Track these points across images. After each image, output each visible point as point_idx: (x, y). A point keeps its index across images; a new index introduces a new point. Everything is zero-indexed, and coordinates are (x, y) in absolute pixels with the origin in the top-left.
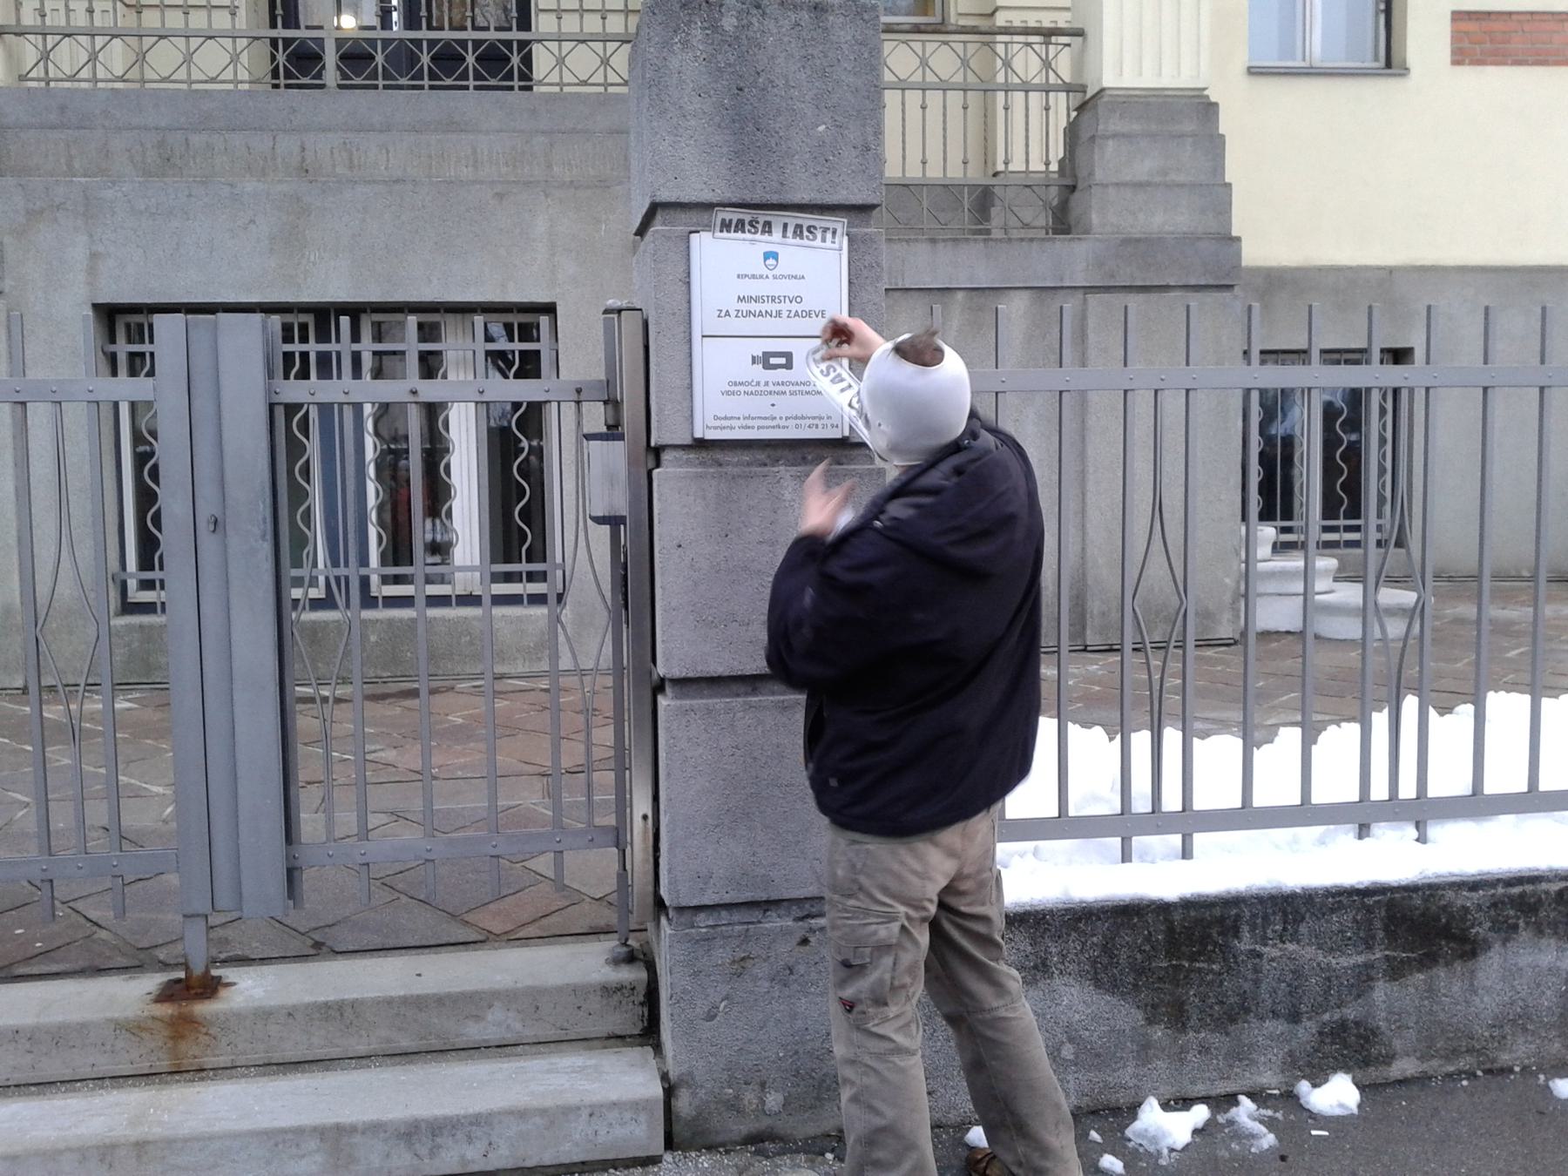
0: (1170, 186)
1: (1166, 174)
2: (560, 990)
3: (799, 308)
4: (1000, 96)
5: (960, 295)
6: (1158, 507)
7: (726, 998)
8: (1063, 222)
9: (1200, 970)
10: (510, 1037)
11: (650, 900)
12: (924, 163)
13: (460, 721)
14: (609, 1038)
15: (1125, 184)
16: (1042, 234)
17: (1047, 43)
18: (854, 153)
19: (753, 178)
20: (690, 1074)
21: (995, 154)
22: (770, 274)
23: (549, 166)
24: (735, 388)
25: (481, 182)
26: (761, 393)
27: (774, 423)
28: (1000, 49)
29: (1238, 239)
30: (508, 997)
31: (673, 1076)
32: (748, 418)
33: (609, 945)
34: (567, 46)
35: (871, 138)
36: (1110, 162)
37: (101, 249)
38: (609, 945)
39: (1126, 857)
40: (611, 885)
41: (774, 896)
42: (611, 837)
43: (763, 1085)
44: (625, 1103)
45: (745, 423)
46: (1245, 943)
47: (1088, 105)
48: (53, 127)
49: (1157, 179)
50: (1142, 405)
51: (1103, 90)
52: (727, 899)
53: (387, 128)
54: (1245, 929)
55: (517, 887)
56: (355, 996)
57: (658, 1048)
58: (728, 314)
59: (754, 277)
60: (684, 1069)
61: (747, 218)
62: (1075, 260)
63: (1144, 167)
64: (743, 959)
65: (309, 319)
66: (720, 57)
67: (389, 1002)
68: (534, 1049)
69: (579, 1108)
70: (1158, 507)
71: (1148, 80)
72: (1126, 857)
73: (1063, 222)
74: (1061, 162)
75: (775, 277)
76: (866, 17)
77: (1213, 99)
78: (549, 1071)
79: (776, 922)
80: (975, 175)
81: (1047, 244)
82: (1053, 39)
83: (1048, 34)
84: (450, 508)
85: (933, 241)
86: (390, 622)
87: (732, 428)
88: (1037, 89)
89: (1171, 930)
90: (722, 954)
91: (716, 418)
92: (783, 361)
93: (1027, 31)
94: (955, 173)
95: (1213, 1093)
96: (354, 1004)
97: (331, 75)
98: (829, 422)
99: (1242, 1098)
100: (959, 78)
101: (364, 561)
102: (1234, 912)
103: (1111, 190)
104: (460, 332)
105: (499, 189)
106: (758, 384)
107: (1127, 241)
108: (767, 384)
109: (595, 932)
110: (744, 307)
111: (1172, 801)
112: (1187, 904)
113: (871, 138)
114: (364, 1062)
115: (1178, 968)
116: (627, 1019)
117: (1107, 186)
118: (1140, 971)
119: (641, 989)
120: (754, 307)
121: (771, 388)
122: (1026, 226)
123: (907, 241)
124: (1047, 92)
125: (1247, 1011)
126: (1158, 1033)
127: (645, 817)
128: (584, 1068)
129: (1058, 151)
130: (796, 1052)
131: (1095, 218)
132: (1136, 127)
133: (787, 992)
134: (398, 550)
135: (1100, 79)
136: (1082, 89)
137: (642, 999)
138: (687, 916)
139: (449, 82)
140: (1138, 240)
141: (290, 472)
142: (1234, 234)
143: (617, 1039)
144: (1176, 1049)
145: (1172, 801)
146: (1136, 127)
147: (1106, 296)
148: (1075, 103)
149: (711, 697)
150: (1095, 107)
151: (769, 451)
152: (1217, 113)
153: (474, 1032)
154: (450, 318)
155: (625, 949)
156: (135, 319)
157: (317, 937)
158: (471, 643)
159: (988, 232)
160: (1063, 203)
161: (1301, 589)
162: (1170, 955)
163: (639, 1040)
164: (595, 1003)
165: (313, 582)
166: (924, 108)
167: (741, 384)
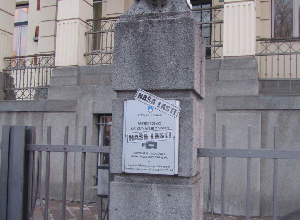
3: (160, 126)
18: (183, 71)
19: (146, 81)
24: (136, 155)
26: (145, 157)
27: (149, 168)
32: (140, 166)
35: (189, 66)
37: (95, 101)
45: (138, 167)
48: (90, 74)
58: (134, 128)
59: (144, 115)
61: (148, 96)
76: (189, 23)
87: (134, 169)
91: (129, 165)
92: (153, 145)
98: (169, 169)
106: (144, 153)
108: (147, 154)
110: (140, 126)
113: (189, 66)
120: (143, 126)
121: (148, 155)
123: (294, 96)
156: (103, 117)
167: (138, 153)
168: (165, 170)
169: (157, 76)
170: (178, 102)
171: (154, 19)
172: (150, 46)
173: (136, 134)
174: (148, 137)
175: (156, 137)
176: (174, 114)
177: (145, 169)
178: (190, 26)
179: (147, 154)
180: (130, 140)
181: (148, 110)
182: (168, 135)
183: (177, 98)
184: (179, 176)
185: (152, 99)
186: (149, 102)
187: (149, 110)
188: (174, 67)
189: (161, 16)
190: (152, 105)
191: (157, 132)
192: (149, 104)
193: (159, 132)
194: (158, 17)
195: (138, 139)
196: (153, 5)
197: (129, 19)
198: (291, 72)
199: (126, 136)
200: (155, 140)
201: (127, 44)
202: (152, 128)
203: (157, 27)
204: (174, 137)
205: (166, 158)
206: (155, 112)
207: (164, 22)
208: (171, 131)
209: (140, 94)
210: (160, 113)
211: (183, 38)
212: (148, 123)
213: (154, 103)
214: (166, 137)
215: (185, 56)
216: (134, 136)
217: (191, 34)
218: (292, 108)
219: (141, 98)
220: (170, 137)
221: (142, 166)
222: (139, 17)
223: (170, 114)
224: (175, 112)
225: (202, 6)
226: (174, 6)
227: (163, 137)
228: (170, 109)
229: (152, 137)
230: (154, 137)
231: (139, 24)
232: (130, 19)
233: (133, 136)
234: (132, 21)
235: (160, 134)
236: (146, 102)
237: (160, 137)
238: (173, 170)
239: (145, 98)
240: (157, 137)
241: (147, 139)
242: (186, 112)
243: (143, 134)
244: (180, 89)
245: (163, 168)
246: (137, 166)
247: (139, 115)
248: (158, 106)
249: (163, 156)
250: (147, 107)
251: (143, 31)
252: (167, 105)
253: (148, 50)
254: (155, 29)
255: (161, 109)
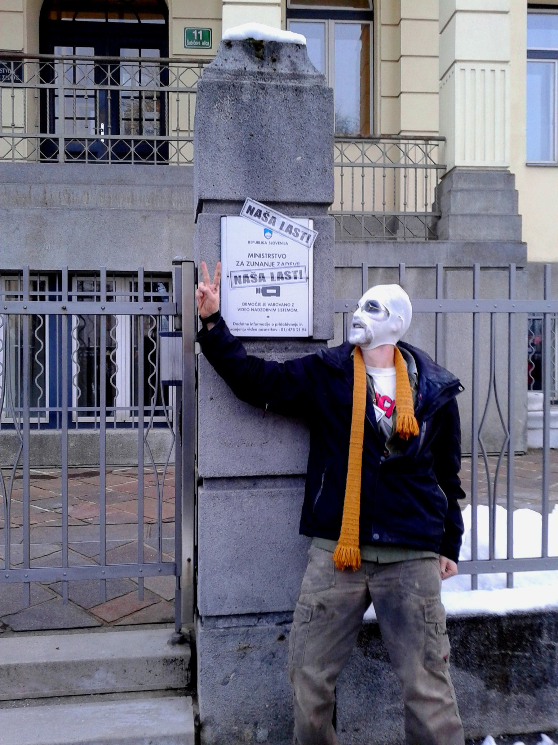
0: (489, 216)
1: (487, 210)
2: (139, 661)
3: (284, 261)
4: (402, 170)
5: (381, 270)
6: (493, 381)
7: (235, 671)
8: (434, 234)
9: (518, 657)
10: (108, 688)
11: (191, 609)
12: (363, 204)
13: (111, 490)
14: (167, 689)
15: (466, 215)
16: (423, 240)
17: (426, 144)
19: (258, 186)
20: (212, 717)
21: (399, 192)
22: (268, 241)
23: (171, 203)
24: (245, 307)
25: (135, 210)
26: (262, 310)
27: (269, 327)
28: (402, 147)
29: (525, 244)
30: (109, 664)
31: (202, 718)
33: (169, 632)
34: (181, 143)
36: (457, 204)
38: (169, 632)
39: (474, 586)
40: (172, 595)
41: (265, 610)
42: (172, 569)
43: (256, 724)
44: (171, 736)
45: (251, 327)
46: (545, 640)
47: (447, 175)
49: (483, 212)
50: (483, 322)
51: (455, 167)
52: (236, 612)
53: (88, 183)
54: (545, 632)
55: (125, 592)
56: (17, 662)
57: (195, 697)
59: (258, 242)
60: (208, 714)
62: (440, 253)
63: (477, 206)
64: (245, 648)
65: (46, 279)
66: (240, 117)
67: (37, 666)
68: (122, 696)
69: (143, 739)
70: (493, 381)
71: (478, 162)
72: (474, 586)
73: (434, 234)
74: (433, 205)
75: (270, 243)
76: (325, 96)
77: (512, 172)
78: (129, 712)
79: (265, 625)
80: (389, 210)
81: (427, 245)
82: (430, 142)
83: (427, 139)
84: (115, 376)
85: (367, 243)
86: (81, 436)
87: (243, 330)
88: (421, 167)
89: (500, 632)
90: (232, 645)
92: (274, 291)
93: (416, 138)
94: (379, 208)
95: (526, 731)
96: (16, 667)
97: (62, 157)
98: (301, 327)
99: (544, 737)
100: (381, 161)
101: (70, 404)
102: (539, 621)
103: (459, 218)
104: (123, 285)
105: (144, 214)
106: (260, 304)
107: (468, 244)
108: (265, 304)
109: (165, 622)
110: (252, 260)
111: (501, 553)
112: (512, 617)
114: (20, 703)
115: (505, 656)
116: (177, 679)
117: (457, 215)
118: (482, 657)
119: (187, 661)
120: (257, 260)
121: (267, 307)
122: (415, 236)
123: (353, 243)
124: (426, 169)
125: (546, 681)
126: (493, 694)
127: (189, 560)
128: (149, 711)
129: (432, 199)
130: (277, 705)
131: (451, 232)
132: (472, 186)
133: (271, 668)
134: (87, 399)
135: (454, 162)
136: (445, 168)
137: (187, 667)
138: (210, 623)
139: (121, 160)
140: (473, 244)
141: (32, 356)
142: (523, 241)
143: (172, 691)
144: (503, 705)
145: (501, 553)
146: (472, 186)
147: (456, 272)
148: (441, 175)
149: (227, 489)
150: (451, 176)
151: (267, 344)
152: (513, 179)
153: (87, 685)
154: (118, 280)
155: (179, 636)
157: (5, 621)
158: (123, 447)
159: (395, 239)
160: (434, 226)
161: (542, 426)
162: (500, 647)
163: (184, 692)
164: (159, 669)
165: (42, 414)
166: (363, 176)
168: (294, 330)
169: (275, 179)
170: (311, 222)
171: (265, 81)
172: (262, 127)
173: (245, 273)
174: (266, 279)
175: (278, 278)
176: (307, 242)
177: (262, 330)
178: (327, 100)
179: (265, 304)
180: (236, 283)
181: (264, 234)
182: (298, 275)
183: (311, 217)
184: (315, 338)
185: (271, 216)
186: (266, 221)
187: (266, 234)
188: (302, 165)
189: (278, 78)
190: (271, 226)
191: (280, 270)
192: (266, 224)
193: (283, 271)
194: (272, 79)
195: (249, 282)
196: (258, 57)
197: (221, 76)
198: (344, 200)
199: (228, 277)
200: (277, 282)
201: (222, 120)
202: (272, 264)
203: (273, 96)
204: (308, 278)
205: (296, 310)
206: (276, 237)
207: (285, 89)
208: (303, 269)
209: (250, 207)
210: (284, 240)
211: (317, 119)
212: (265, 255)
213: (274, 222)
214: (295, 278)
215: (321, 149)
216: (242, 276)
217: (330, 114)
218: (350, 266)
219: (251, 214)
220: (301, 278)
221: (256, 325)
222: (239, 75)
223: (300, 241)
224: (308, 239)
225: (77, 48)
226: (293, 63)
227: (290, 278)
228: (301, 234)
229: (272, 277)
230: (276, 278)
231: (241, 88)
232: (224, 76)
233: (240, 277)
234: (230, 81)
235: (285, 273)
236: (260, 220)
237: (286, 278)
238: (307, 329)
239: (259, 214)
240: (280, 277)
241: (265, 281)
242: (323, 238)
243: (257, 273)
244: (313, 201)
245: (291, 327)
246: (248, 324)
247: (249, 242)
248: (281, 229)
249: (290, 308)
250: (262, 229)
251: (250, 100)
252: (295, 226)
253: (260, 133)
254: (271, 100)
255: (285, 233)
